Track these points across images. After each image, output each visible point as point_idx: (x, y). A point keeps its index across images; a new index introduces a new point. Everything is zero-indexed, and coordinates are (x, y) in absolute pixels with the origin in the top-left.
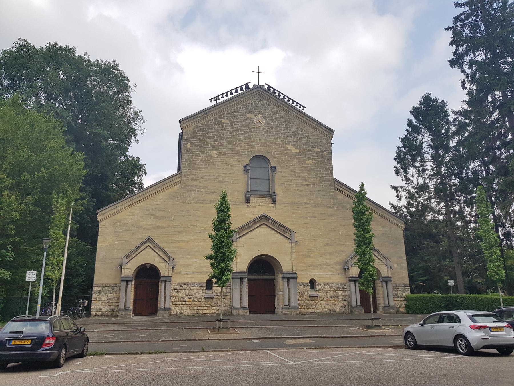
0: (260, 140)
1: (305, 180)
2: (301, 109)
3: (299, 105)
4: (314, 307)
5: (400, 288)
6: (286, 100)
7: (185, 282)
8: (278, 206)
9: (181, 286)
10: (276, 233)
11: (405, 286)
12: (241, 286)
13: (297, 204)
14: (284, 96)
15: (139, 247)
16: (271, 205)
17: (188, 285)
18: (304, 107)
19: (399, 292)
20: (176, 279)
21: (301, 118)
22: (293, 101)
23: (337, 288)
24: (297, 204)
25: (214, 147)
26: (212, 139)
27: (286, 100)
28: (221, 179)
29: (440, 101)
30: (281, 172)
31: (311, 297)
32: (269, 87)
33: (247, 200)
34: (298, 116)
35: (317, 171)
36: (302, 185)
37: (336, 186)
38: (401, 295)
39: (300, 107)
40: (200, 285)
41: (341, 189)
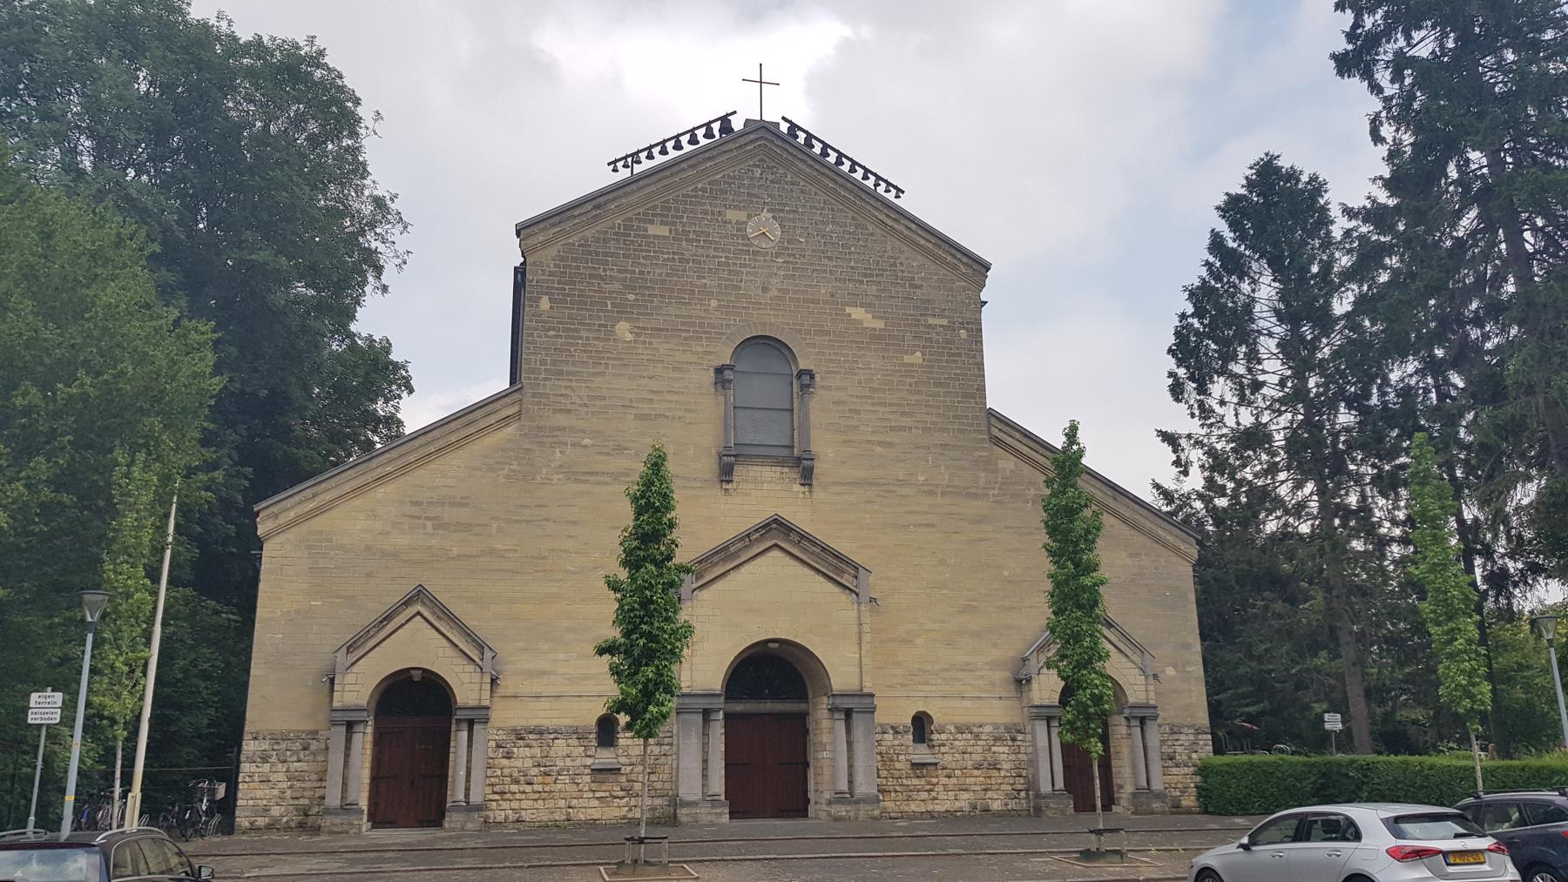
0: (765, 289)
1: (903, 414)
2: (891, 196)
3: (872, 178)
4: (924, 795)
5: (1183, 737)
6: (846, 167)
7: (532, 723)
8: (818, 493)
9: (518, 735)
10: (812, 573)
11: (1198, 731)
12: (705, 745)
13: (877, 485)
14: (840, 155)
15: (388, 618)
16: (797, 488)
17: (540, 732)
18: (899, 191)
19: (1179, 749)
20: (505, 716)
21: (889, 222)
22: (867, 171)
23: (996, 739)
24: (877, 485)
25: (623, 311)
26: (617, 286)
27: (846, 167)
28: (645, 408)
29: (1305, 178)
30: (830, 388)
31: (915, 766)
32: (794, 127)
33: (726, 473)
34: (882, 217)
35: (937, 385)
36: (893, 429)
37: (995, 432)
38: (1185, 757)
39: (887, 191)
40: (579, 734)
41: (1009, 440)
